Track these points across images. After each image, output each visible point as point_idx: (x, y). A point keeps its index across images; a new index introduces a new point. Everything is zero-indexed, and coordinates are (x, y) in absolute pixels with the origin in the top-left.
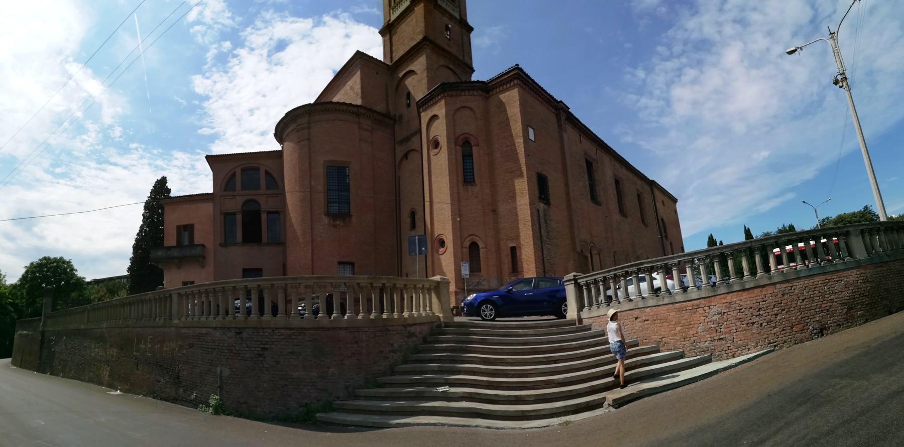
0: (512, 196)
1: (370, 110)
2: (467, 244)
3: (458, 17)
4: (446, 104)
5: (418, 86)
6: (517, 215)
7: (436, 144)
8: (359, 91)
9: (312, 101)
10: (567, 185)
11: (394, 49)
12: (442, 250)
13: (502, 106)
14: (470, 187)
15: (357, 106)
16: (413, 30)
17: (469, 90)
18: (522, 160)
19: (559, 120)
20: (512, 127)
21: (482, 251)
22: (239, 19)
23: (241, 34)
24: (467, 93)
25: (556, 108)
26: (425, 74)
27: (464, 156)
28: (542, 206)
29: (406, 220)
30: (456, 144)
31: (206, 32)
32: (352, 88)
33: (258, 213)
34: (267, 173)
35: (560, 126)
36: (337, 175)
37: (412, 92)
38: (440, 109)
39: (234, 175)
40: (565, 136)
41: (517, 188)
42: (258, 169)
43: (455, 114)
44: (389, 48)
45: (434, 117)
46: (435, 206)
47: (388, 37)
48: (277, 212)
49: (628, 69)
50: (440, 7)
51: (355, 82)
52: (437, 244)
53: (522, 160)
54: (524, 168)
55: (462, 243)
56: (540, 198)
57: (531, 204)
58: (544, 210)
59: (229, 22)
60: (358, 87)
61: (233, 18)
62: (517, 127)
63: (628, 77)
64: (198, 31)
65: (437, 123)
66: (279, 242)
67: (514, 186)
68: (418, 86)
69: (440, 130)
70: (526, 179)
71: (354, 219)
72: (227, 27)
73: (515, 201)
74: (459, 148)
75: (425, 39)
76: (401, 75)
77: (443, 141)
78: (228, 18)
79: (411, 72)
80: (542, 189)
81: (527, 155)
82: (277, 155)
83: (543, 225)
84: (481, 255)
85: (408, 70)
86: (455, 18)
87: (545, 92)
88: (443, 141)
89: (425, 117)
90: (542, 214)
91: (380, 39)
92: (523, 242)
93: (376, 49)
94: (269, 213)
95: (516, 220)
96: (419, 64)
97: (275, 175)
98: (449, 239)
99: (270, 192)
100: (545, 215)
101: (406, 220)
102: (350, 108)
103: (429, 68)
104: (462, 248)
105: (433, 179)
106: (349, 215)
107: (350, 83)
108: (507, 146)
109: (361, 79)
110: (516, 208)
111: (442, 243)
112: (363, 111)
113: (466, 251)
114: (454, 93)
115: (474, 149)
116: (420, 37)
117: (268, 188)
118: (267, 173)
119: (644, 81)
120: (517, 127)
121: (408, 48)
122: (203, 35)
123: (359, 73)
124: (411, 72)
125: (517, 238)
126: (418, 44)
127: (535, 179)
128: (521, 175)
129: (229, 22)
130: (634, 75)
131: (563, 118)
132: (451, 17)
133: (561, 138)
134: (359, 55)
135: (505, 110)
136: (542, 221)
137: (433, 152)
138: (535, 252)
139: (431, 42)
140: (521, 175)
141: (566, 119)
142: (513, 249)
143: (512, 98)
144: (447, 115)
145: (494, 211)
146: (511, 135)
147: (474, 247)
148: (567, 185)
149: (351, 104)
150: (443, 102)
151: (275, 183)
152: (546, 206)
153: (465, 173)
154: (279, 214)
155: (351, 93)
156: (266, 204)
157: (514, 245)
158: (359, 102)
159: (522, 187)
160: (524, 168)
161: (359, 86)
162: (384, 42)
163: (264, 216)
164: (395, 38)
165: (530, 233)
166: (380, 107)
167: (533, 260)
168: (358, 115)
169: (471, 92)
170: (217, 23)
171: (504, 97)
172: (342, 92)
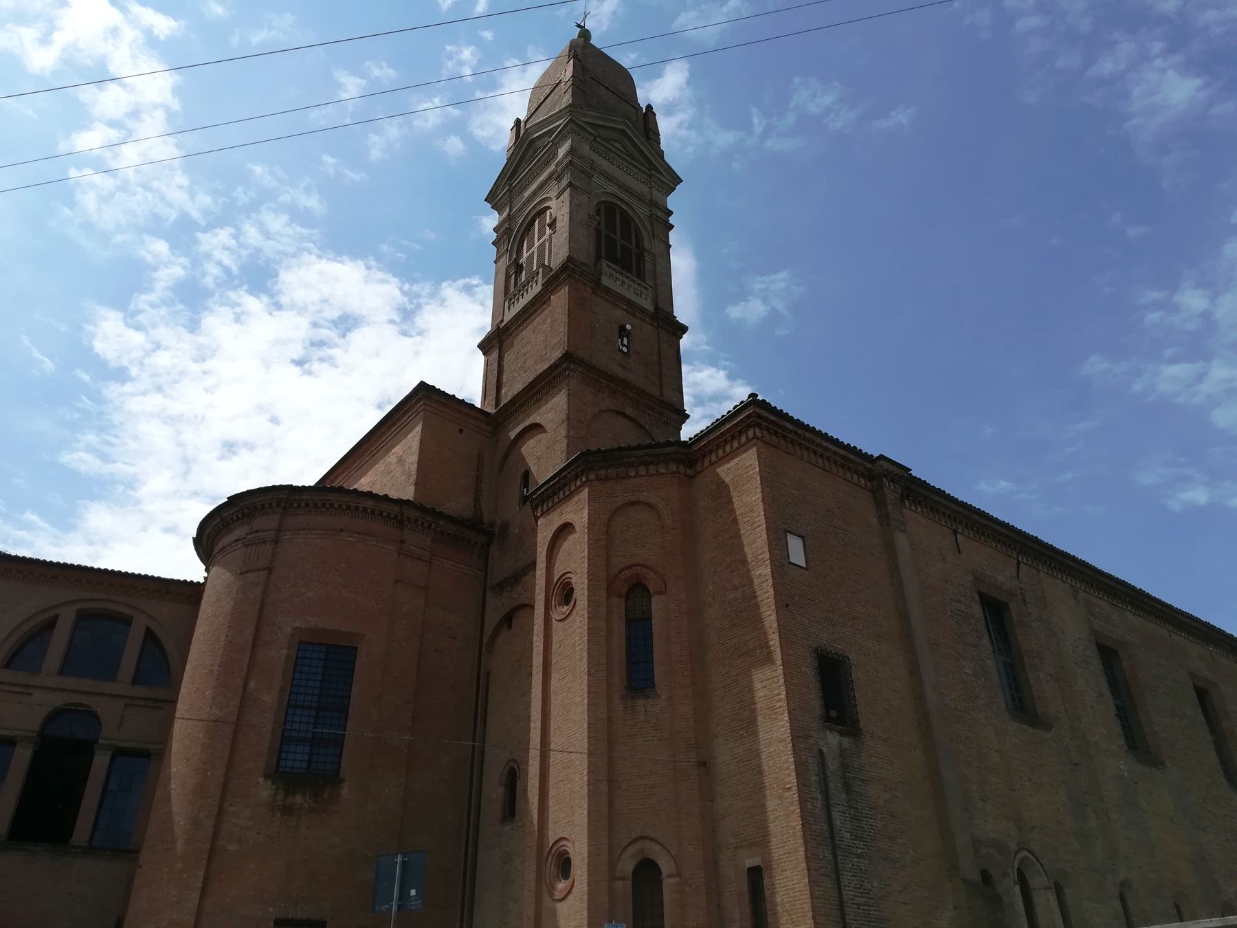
0: (748, 723)
1: (432, 512)
2: (627, 865)
3: (651, 309)
4: (591, 499)
5: (544, 456)
6: (760, 773)
7: (567, 593)
8: (414, 468)
9: (310, 478)
10: (914, 671)
11: (505, 379)
12: (562, 885)
13: (722, 493)
14: (640, 703)
15: (399, 502)
16: (545, 342)
17: (647, 464)
18: (770, 619)
19: (880, 503)
20: (745, 540)
21: (668, 884)
22: (205, 200)
23: (199, 235)
24: (642, 470)
25: (870, 476)
26: (563, 432)
27: (630, 622)
28: (832, 741)
29: (494, 792)
30: (610, 593)
31: (112, 195)
32: (400, 461)
33: (86, 749)
34: (149, 635)
35: (884, 519)
36: (326, 666)
37: (534, 470)
38: (577, 511)
39: (51, 624)
40: (901, 541)
41: (759, 694)
42: (127, 621)
43: (611, 519)
44: (495, 379)
45: (566, 528)
46: (554, 758)
47: (495, 354)
48: (145, 754)
49: (1156, 295)
50: (608, 290)
51: (407, 447)
52: (551, 867)
53: (770, 619)
54: (774, 641)
55: (612, 865)
56: (827, 719)
57: (798, 736)
58: (843, 753)
59: (179, 197)
60: (412, 459)
61: (192, 196)
62: (755, 540)
63: (1154, 317)
64: (93, 186)
65: (568, 546)
66: (121, 847)
67: (751, 690)
68: (544, 456)
69: (575, 560)
70: (780, 670)
71: (345, 791)
72: (170, 205)
73: (755, 734)
74: (618, 604)
75: (567, 357)
76: (513, 434)
77: (580, 584)
78: (181, 187)
79: (536, 428)
80: (832, 691)
81: (783, 604)
82: (188, 592)
83: (839, 796)
84: (667, 897)
85: (527, 422)
86: (643, 310)
87: (836, 442)
88: (580, 584)
89: (546, 529)
90: (832, 765)
91: (480, 358)
92: (777, 851)
93: (466, 379)
94: (119, 753)
95: (758, 788)
96: (553, 412)
97: (170, 646)
98: (579, 851)
99: (141, 691)
100: (844, 767)
101: (494, 792)
102: (383, 506)
103: (573, 420)
104: (613, 878)
105: (554, 683)
106: (335, 779)
107: (398, 450)
108: (735, 588)
109: (421, 442)
110: (757, 753)
111: (564, 866)
112: (414, 514)
113: (624, 887)
114: (612, 472)
115: (657, 604)
116: (558, 354)
117: (135, 681)
118: (149, 635)
119: (1206, 316)
120: (755, 540)
121: (531, 377)
122: (105, 199)
123: (419, 428)
124: (536, 428)
125: (762, 841)
126: (553, 368)
127: (809, 670)
128: (768, 659)
129: (179, 197)
130: (1173, 308)
131: (891, 492)
132: (633, 308)
133: (890, 547)
134: (424, 392)
135: (730, 501)
136: (835, 785)
137: (560, 611)
138: (812, 883)
139: (582, 362)
140: (768, 659)
141: (904, 497)
142: (756, 876)
143: (743, 472)
144: (591, 524)
145: (704, 765)
146: (744, 561)
147: (647, 872)
148: (914, 671)
149: (386, 498)
150: (585, 493)
151: (160, 669)
152: (846, 742)
153: (631, 666)
154: (144, 759)
155: (394, 477)
156: (118, 724)
157: (754, 861)
158: (408, 493)
159: (770, 689)
160: (774, 641)
161: (415, 458)
162: (487, 365)
163: (100, 762)
164: (509, 357)
165: (797, 823)
166: (459, 505)
167: (807, 907)
168: (400, 522)
169: (652, 469)
170: (146, 187)
171: (726, 471)
172: (380, 466)
